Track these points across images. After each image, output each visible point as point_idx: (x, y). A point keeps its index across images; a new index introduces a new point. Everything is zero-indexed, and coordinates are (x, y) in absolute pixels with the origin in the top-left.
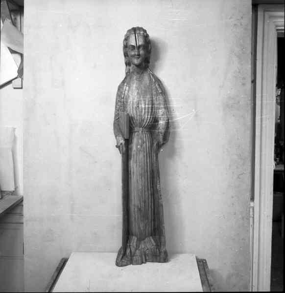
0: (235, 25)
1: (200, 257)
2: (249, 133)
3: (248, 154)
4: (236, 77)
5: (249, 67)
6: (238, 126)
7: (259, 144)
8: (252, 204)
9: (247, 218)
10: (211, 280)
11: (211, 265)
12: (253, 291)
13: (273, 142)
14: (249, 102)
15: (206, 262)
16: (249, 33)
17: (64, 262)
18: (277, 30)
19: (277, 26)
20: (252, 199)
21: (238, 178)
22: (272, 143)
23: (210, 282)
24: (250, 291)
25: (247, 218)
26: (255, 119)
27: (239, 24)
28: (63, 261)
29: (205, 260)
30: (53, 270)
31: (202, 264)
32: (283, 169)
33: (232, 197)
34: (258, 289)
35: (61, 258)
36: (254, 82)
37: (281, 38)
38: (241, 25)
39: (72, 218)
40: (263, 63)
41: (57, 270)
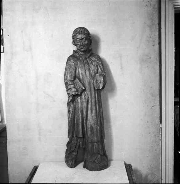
0: (147, 5)
1: (128, 163)
2: (158, 78)
3: (157, 93)
4: (148, 41)
5: (157, 33)
6: (151, 73)
7: (166, 81)
8: (161, 125)
9: (158, 133)
10: (135, 180)
11: (134, 166)
12: (162, 183)
13: (174, 92)
14: (158, 58)
15: (131, 166)
16: (157, 10)
17: (36, 169)
18: (175, 8)
19: (174, 6)
20: (161, 122)
21: (151, 108)
22: (173, 26)
23: (134, 180)
24: (161, 183)
25: (158, 133)
26: (161, 102)
27: (149, 5)
28: (35, 168)
29: (131, 165)
30: (28, 174)
31: (128, 168)
32: (178, 100)
33: (147, 122)
34: (165, 182)
35: (34, 166)
36: (160, 43)
37: (177, 14)
38: (151, 5)
39: (40, 139)
40: (166, 158)
41: (30, 174)
